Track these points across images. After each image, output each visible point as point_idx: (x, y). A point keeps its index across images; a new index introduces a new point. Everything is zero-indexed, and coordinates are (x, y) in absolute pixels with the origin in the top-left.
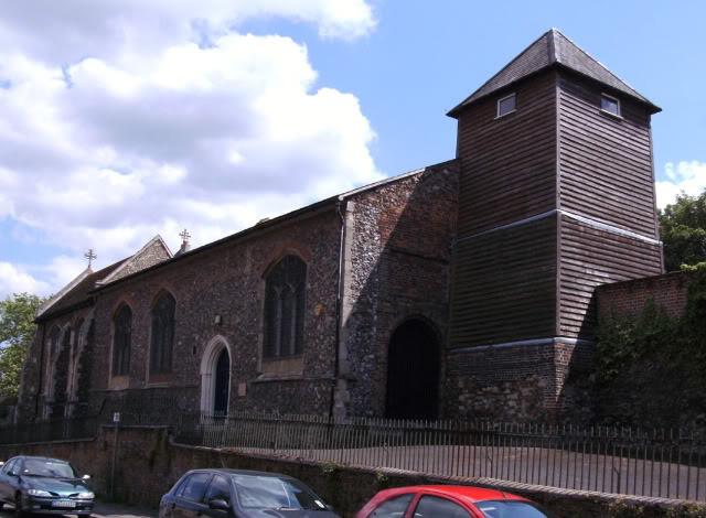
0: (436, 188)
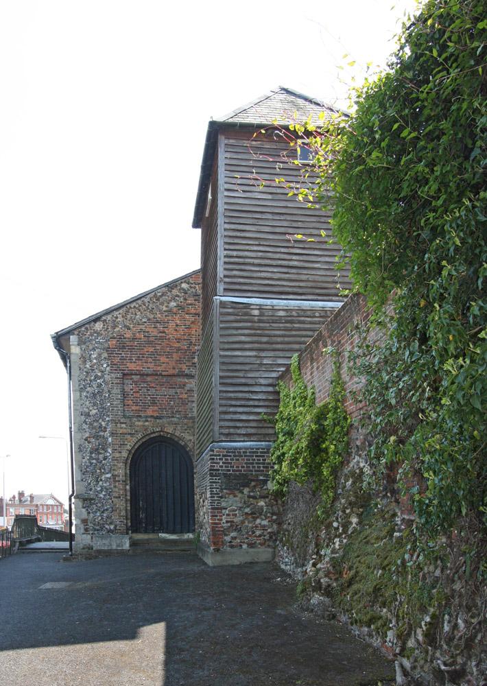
0: (173, 304)
